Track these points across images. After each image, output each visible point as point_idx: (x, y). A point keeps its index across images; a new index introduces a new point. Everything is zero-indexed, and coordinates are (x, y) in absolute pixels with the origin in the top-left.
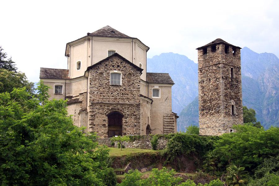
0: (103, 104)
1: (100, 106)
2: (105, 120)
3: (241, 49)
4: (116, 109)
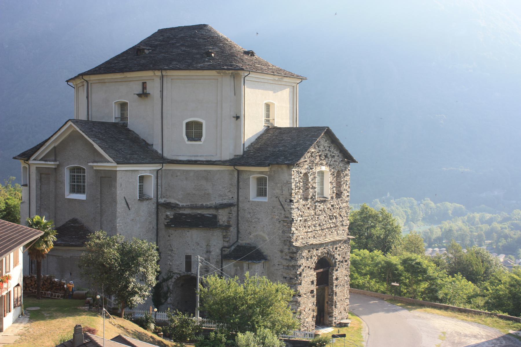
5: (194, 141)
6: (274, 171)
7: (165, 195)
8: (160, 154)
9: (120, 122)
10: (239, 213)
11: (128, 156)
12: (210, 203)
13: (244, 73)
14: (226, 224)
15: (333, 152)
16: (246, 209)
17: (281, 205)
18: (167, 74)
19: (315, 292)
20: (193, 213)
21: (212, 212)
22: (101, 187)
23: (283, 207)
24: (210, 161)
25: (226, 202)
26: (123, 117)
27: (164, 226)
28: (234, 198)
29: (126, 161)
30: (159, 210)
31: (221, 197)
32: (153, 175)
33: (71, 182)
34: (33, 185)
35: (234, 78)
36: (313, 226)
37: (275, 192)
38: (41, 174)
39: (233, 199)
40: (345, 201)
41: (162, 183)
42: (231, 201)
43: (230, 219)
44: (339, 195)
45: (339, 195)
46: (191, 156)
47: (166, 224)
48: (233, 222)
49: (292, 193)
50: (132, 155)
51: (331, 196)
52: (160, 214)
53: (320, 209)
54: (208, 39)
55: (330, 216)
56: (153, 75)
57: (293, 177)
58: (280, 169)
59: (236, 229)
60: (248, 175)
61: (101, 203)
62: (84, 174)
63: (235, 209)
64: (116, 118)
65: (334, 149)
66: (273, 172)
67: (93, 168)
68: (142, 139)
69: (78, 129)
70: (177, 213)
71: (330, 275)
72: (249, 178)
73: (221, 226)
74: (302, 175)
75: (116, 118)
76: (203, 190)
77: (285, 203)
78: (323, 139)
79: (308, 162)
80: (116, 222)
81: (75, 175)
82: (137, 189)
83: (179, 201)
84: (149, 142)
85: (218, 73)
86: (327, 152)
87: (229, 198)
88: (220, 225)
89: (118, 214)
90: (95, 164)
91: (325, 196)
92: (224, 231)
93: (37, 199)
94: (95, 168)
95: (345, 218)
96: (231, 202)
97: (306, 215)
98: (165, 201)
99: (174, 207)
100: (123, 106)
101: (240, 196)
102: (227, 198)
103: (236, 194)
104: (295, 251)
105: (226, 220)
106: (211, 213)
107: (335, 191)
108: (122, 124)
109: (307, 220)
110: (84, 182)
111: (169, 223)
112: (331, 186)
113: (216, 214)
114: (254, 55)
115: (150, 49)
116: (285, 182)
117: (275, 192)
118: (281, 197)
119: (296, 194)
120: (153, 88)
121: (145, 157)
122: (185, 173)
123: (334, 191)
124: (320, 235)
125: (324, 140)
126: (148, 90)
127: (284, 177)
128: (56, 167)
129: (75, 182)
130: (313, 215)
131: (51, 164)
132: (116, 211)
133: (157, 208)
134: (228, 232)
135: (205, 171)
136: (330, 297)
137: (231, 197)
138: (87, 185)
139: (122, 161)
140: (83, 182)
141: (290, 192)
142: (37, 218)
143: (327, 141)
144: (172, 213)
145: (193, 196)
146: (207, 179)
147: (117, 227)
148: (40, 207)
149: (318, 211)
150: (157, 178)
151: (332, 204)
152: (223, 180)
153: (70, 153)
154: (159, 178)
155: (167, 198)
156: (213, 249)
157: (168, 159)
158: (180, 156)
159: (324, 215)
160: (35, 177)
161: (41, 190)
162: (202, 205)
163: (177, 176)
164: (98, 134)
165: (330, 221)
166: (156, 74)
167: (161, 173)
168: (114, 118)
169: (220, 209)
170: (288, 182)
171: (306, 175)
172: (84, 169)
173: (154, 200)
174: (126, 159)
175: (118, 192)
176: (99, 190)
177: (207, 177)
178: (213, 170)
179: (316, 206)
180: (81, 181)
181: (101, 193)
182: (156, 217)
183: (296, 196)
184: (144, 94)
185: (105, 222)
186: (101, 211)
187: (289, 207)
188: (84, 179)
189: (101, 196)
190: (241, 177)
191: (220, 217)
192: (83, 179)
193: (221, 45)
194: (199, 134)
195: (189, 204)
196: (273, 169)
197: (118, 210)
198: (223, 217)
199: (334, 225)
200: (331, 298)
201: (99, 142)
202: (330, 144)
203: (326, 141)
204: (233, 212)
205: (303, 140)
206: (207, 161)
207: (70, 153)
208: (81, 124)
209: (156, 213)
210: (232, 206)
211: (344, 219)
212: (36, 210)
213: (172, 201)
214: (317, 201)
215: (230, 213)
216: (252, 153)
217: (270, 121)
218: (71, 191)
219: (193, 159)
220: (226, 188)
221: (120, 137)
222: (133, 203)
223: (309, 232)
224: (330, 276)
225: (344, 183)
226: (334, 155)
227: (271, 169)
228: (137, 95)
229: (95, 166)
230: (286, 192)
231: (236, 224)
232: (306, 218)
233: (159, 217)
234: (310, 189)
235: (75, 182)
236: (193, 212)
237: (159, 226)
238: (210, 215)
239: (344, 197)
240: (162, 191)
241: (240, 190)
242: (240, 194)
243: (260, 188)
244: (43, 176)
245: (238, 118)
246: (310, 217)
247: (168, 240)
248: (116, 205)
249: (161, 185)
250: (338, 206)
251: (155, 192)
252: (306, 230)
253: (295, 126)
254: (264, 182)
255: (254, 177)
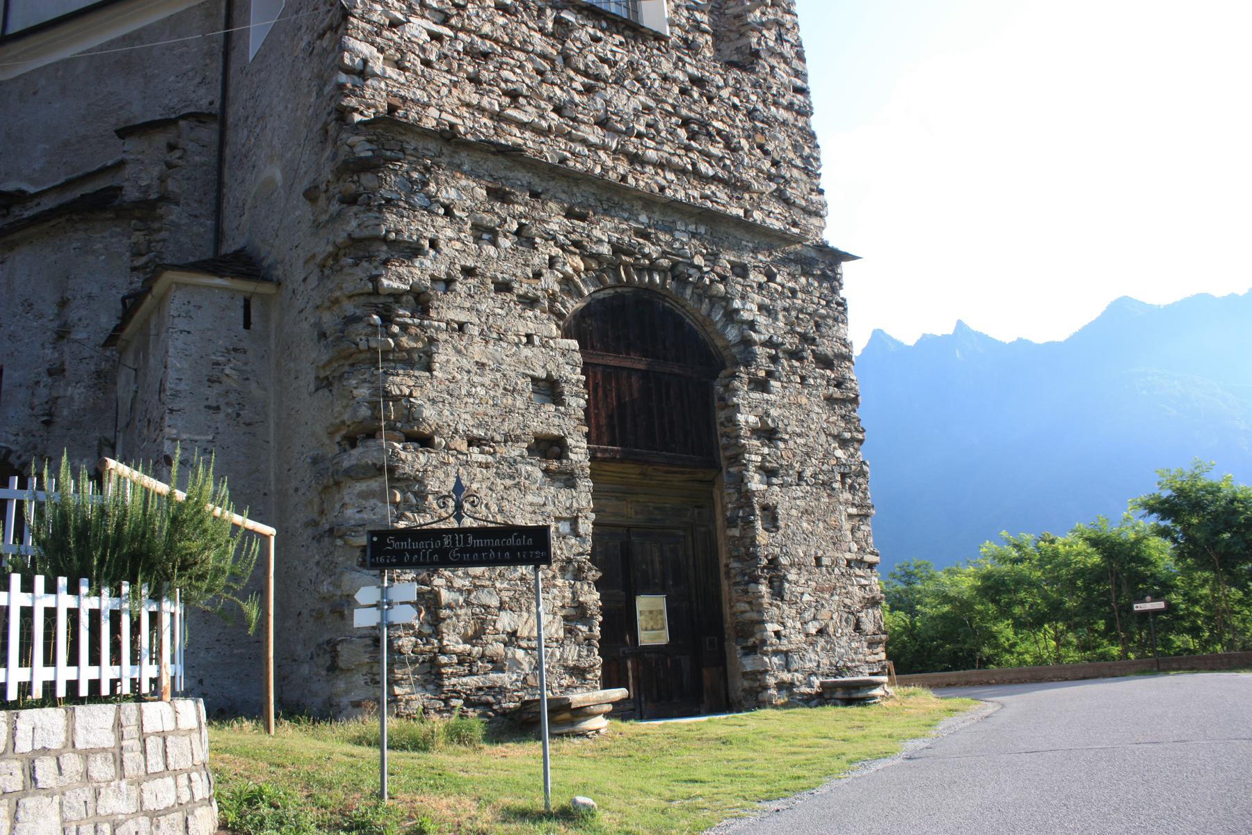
0: (523, 176)
1: (481, 193)
2: (550, 389)
3: (845, 267)
4: (653, 267)
19: (579, 453)
71: (723, 409)
104: (364, 150)
122: (60, 73)
136: (736, 532)
156: (83, 313)
163: (35, 93)
178: (150, 26)
200: (742, 537)
220: (190, 74)
224: (721, 415)
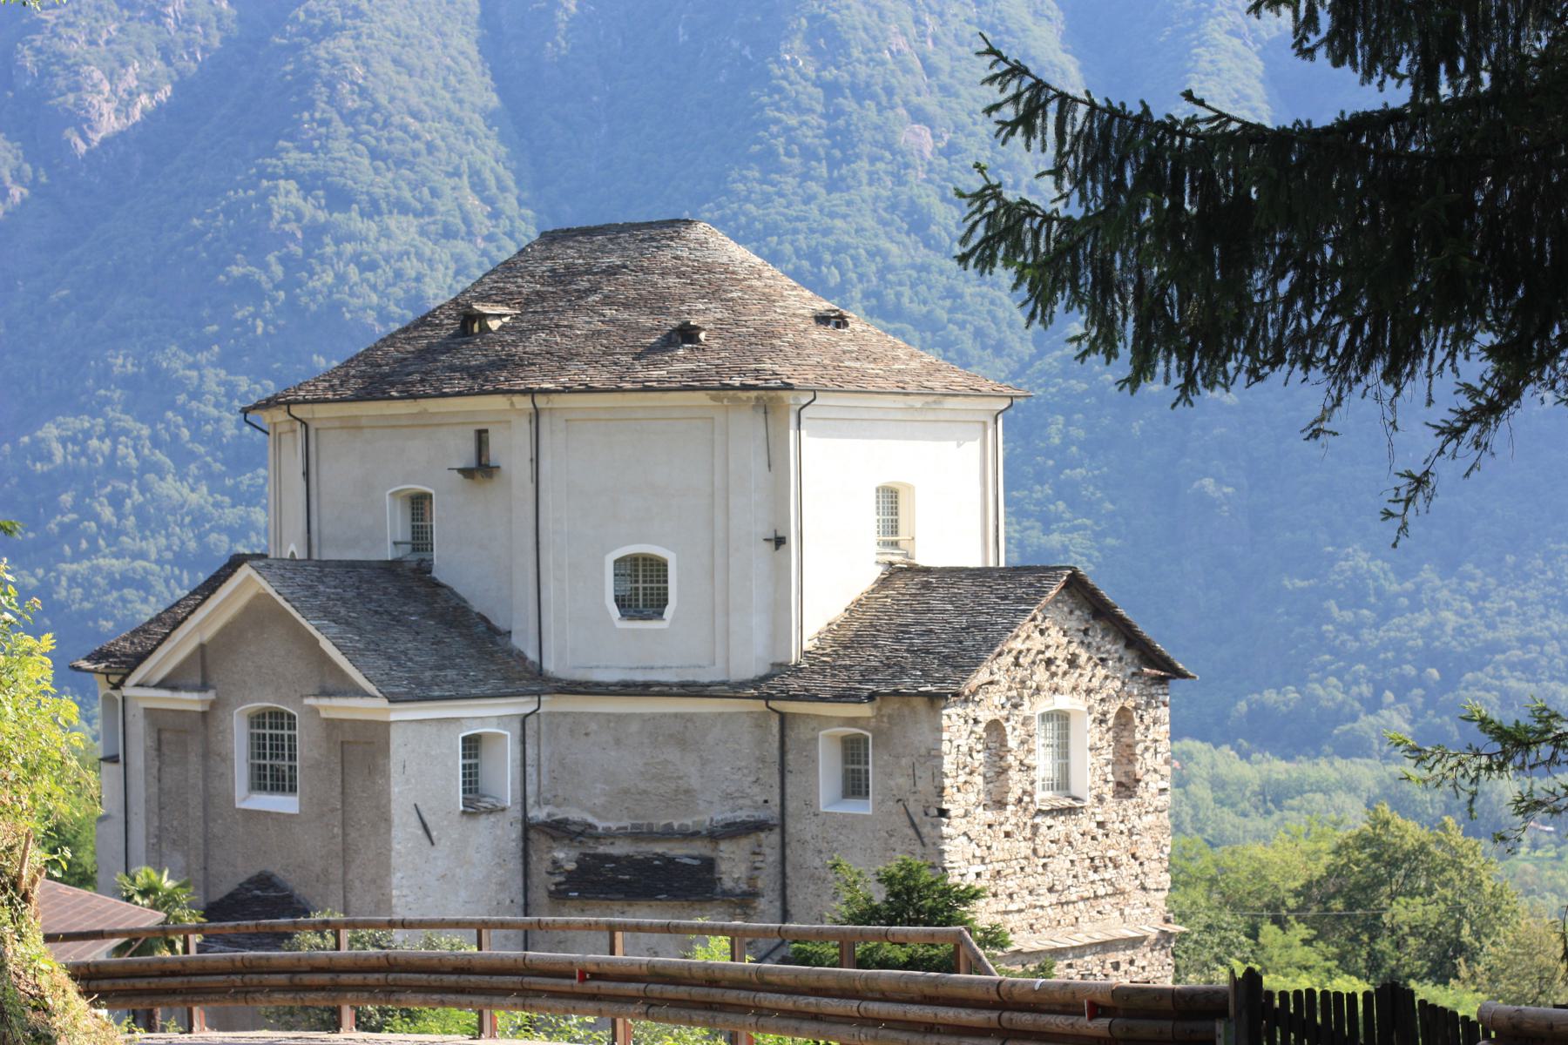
5: (642, 619)
6: (890, 717)
7: (549, 796)
8: (533, 663)
9: (409, 558)
10: (788, 852)
11: (428, 674)
12: (696, 819)
13: (796, 398)
14: (745, 887)
15: (1098, 649)
16: (808, 837)
17: (913, 825)
18: (549, 406)
20: (639, 853)
21: (700, 848)
22: (343, 773)
23: (918, 833)
24: (694, 684)
25: (744, 818)
26: (421, 538)
27: (545, 894)
28: (771, 804)
29: (417, 691)
30: (530, 844)
31: (731, 802)
32: (508, 733)
33: (252, 758)
34: (138, 760)
35: (766, 413)
36: (1025, 892)
37: (892, 783)
38: (159, 731)
39: (769, 808)
40: (1151, 809)
41: (539, 755)
42: (760, 815)
43: (756, 873)
44: (1126, 787)
45: (1126, 787)
46: (631, 669)
47: (553, 888)
48: (767, 881)
49: (943, 789)
50: (440, 670)
51: (1094, 792)
52: (534, 858)
53: (1053, 834)
54: (695, 276)
55: (1092, 859)
56: (508, 407)
57: (945, 736)
58: (906, 711)
59: (778, 904)
60: (813, 729)
61: (344, 825)
62: (291, 732)
63: (774, 838)
64: (395, 543)
65: (1103, 638)
66: (885, 719)
67: (318, 712)
68: (478, 614)
69: (272, 592)
70: (588, 855)
72: (816, 739)
73: (727, 894)
74: (980, 729)
75: (395, 543)
76: (670, 778)
77: (925, 818)
78: (1060, 605)
79: (1004, 683)
80: (390, 884)
81: (264, 735)
82: (457, 779)
83: (595, 814)
84: (499, 622)
85: (713, 398)
86: (1073, 648)
87: (756, 802)
88: (725, 893)
89: (395, 860)
90: (324, 702)
91: (1074, 793)
92: (738, 911)
93: (148, 811)
94: (324, 714)
95: (1154, 865)
96: (762, 818)
97: (1000, 856)
98: (549, 815)
99: (580, 834)
100: (419, 504)
101: (788, 797)
102: (748, 802)
103: (777, 791)
105: (744, 876)
106: (695, 853)
107: (1110, 777)
108: (414, 565)
109: (1003, 873)
110: (292, 757)
111: (563, 887)
112: (1094, 760)
113: (713, 855)
114: (846, 325)
115: (505, 315)
116: (923, 751)
117: (892, 783)
118: (912, 799)
119: (959, 790)
120: (510, 449)
121: (481, 676)
122: (612, 725)
123: (1105, 774)
124: (1055, 923)
125: (1066, 609)
126: (495, 453)
127: (919, 736)
128: (206, 708)
129: (265, 758)
130: (1026, 858)
131: (190, 701)
132: (390, 850)
133: (525, 838)
134: (752, 912)
135: (676, 715)
137: (760, 799)
138: (302, 767)
139: (407, 693)
140: (290, 756)
141: (936, 783)
142: (144, 874)
143: (1078, 613)
144: (574, 854)
145: (638, 797)
146: (682, 742)
147: (394, 901)
148: (159, 837)
149: (1043, 844)
150: (523, 742)
151: (1100, 818)
152: (736, 746)
153: (249, 663)
154: (528, 741)
155: (558, 806)
157: (559, 680)
158: (597, 667)
159: (1071, 857)
160: (142, 731)
161: (159, 781)
162: (669, 826)
164: (335, 605)
165: (1092, 876)
166: (518, 406)
167: (535, 725)
168: (389, 543)
169: (724, 839)
170: (933, 753)
171: (995, 727)
172: (291, 717)
173: (515, 813)
174: (420, 684)
175: (395, 790)
176: (339, 782)
177: (682, 734)
179: (1035, 827)
180: (283, 755)
181: (343, 793)
182: (520, 867)
183: (959, 797)
184: (481, 469)
185: (357, 883)
186: (344, 850)
187: (934, 833)
188: (292, 748)
189: (343, 802)
190: (792, 735)
191: (723, 866)
192: (290, 746)
193: (734, 295)
194: (659, 594)
195: (626, 823)
196: (887, 711)
197: (396, 846)
198: (733, 864)
199: (1110, 890)
201: (335, 629)
202: (1087, 621)
203: (1071, 612)
204: (767, 850)
205: (988, 614)
206: (683, 685)
207: (249, 663)
208: (282, 571)
209: (520, 854)
210: (762, 830)
211: (1146, 869)
212: (147, 846)
213: (574, 814)
214: (1040, 810)
215: (754, 853)
216: (828, 655)
217: (902, 544)
218: (252, 784)
219: (640, 677)
220: (745, 771)
221: (406, 608)
222: (446, 823)
223: (1011, 912)
225: (1147, 749)
226: (1104, 656)
227: (879, 709)
228: (461, 471)
229: (326, 708)
230: (924, 785)
231: (778, 886)
232: (998, 866)
233: (532, 866)
234: (1011, 773)
235: (265, 758)
236: (640, 850)
237: (532, 896)
238: (694, 858)
239: (1146, 796)
240: (539, 781)
241: (790, 778)
242: (789, 790)
243: (853, 770)
244: (166, 736)
245: (780, 541)
246: (1014, 863)
247: (560, 942)
248: (389, 831)
249: (535, 763)
250: (1122, 827)
251: (518, 787)
252: (1001, 908)
253: (991, 564)
254: (863, 752)
255: (830, 736)
